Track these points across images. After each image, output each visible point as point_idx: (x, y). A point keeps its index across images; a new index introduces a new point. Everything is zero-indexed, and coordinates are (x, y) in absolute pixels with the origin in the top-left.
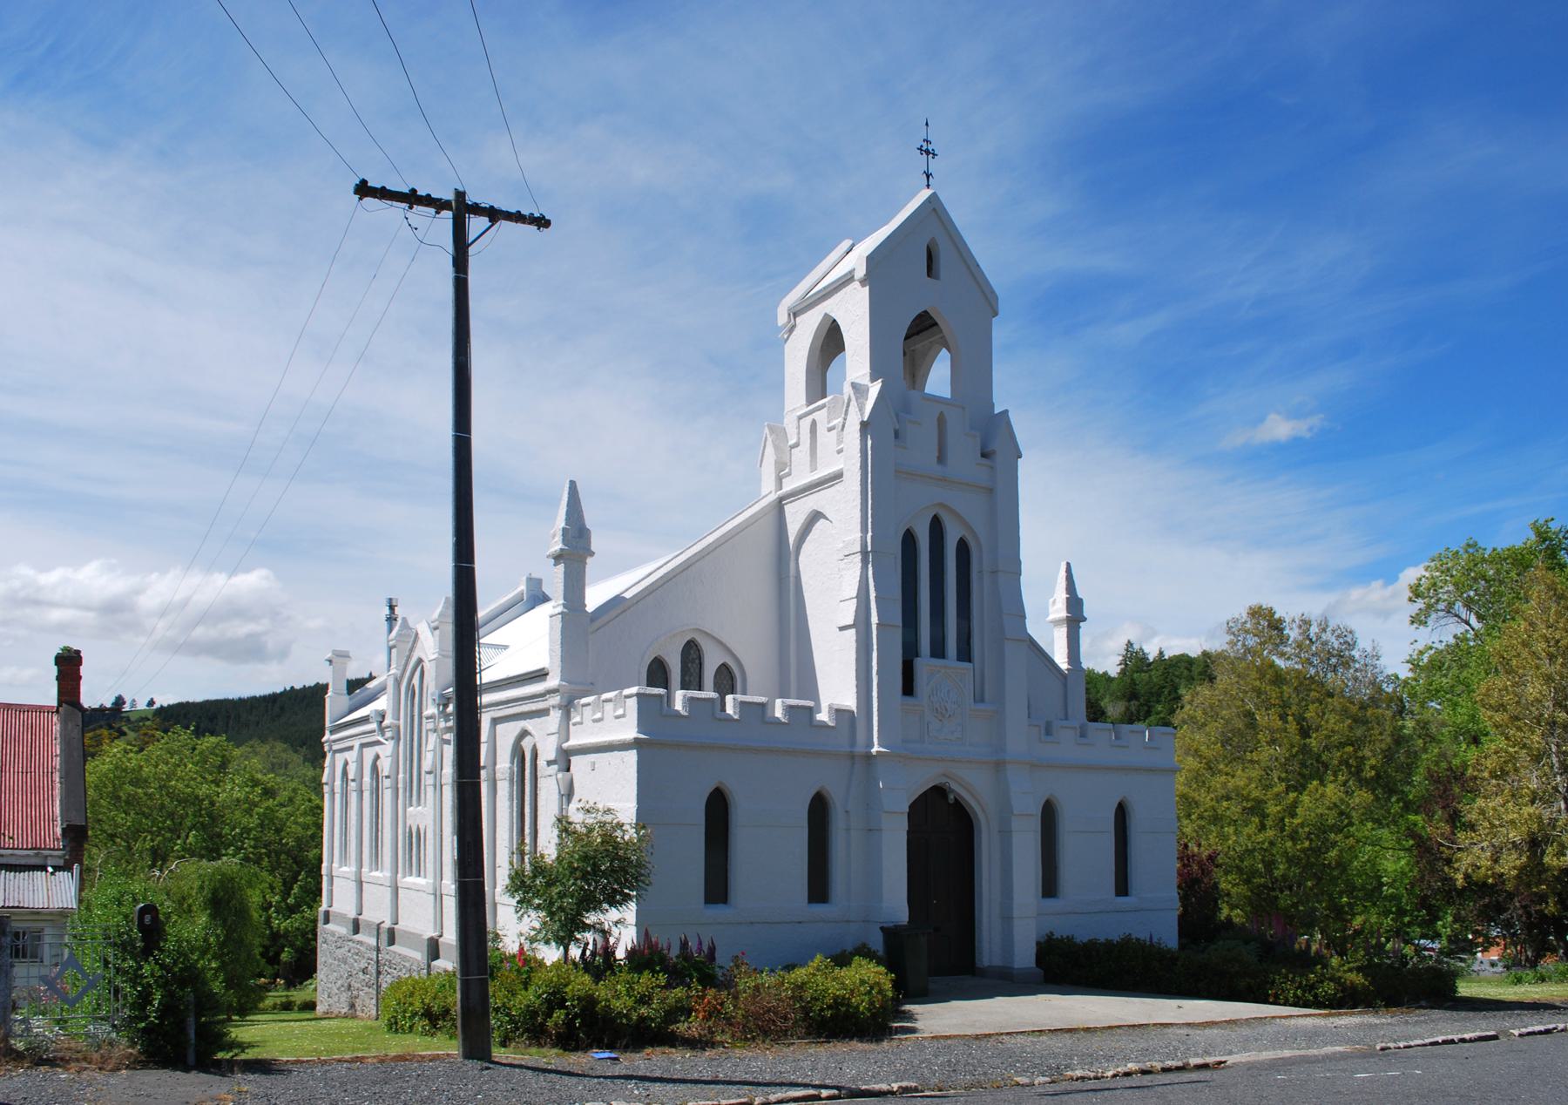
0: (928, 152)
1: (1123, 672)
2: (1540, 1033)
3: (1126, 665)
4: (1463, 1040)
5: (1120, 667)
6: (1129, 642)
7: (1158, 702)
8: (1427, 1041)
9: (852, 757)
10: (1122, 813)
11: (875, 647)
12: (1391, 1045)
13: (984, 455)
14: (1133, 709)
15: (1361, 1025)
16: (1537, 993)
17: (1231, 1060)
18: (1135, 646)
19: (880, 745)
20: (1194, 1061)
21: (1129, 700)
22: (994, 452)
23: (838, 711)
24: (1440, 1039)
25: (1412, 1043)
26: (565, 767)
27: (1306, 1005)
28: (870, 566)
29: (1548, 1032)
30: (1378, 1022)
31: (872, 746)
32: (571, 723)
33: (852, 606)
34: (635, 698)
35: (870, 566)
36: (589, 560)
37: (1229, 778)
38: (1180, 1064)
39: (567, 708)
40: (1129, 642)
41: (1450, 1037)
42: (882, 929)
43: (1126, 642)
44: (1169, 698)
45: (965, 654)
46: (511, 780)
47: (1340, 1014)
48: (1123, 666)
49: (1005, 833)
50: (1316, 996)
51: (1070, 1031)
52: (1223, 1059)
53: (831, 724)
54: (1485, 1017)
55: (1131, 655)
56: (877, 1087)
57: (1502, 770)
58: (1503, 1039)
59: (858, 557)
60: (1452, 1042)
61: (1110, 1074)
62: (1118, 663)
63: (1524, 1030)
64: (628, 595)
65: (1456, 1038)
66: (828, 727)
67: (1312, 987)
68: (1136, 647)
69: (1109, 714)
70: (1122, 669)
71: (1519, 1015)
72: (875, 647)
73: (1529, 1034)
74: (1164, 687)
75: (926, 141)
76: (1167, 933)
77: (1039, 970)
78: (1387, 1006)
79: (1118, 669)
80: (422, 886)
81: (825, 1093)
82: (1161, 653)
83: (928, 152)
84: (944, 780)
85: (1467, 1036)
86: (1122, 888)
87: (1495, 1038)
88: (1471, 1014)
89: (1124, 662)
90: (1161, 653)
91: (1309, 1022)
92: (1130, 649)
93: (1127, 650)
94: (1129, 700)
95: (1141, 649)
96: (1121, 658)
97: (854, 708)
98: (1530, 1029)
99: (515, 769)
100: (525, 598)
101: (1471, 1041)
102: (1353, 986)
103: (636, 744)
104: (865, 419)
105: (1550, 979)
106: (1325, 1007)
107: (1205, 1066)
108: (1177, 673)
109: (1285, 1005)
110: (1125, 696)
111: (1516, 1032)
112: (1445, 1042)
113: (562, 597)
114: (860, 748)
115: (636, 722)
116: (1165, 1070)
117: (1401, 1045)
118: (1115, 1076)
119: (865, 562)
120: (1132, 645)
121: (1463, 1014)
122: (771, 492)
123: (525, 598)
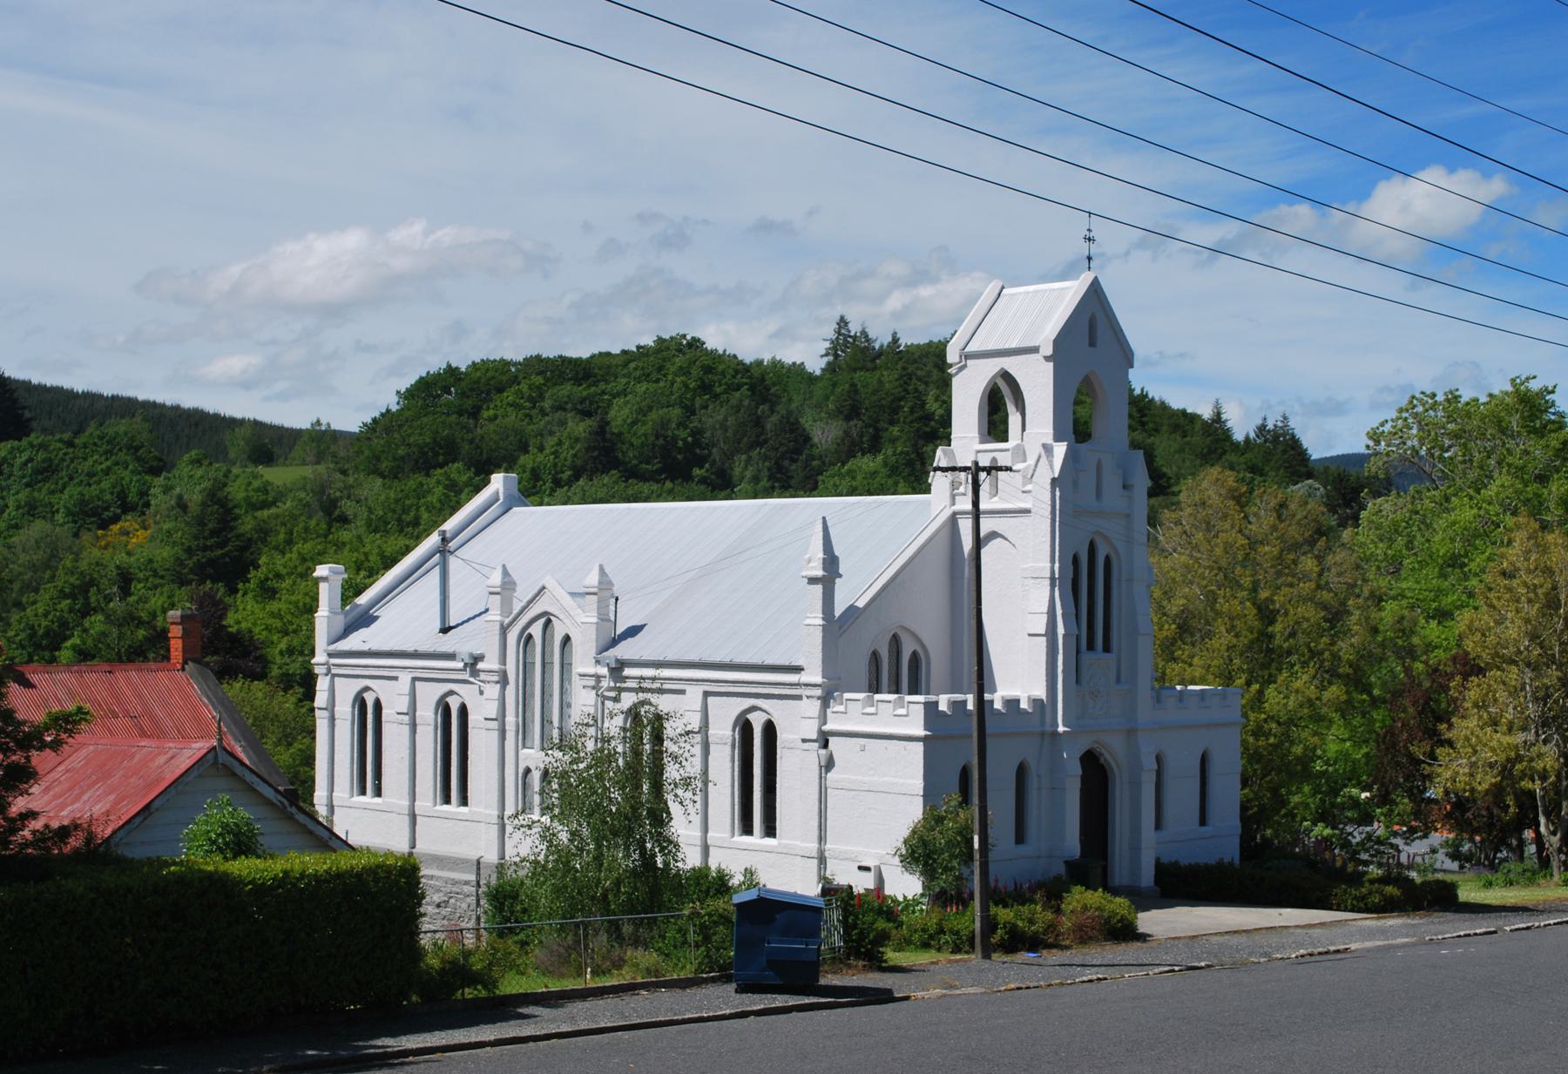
0: (1089, 239)
1: (831, 369)
2: (1523, 929)
3: (836, 356)
4: (1476, 934)
5: (826, 359)
6: (842, 318)
7: (892, 423)
8: (1455, 935)
9: (1043, 734)
10: (1204, 760)
11: (1061, 651)
12: (1434, 937)
13: (1125, 487)
14: (854, 433)
15: (1406, 925)
16: (1511, 898)
17: (1353, 946)
18: (851, 326)
19: (1064, 725)
20: (1332, 948)
21: (848, 418)
22: (1132, 486)
23: (1034, 700)
24: (1462, 933)
25: (1446, 936)
26: (823, 743)
27: (1359, 911)
28: (1057, 589)
29: (1528, 928)
30: (1413, 922)
31: (1058, 726)
32: (829, 711)
33: (1044, 619)
34: (922, 706)
35: (1057, 589)
36: (838, 581)
37: (1186, 666)
38: (1325, 950)
39: (826, 700)
40: (842, 318)
41: (1467, 932)
42: (1066, 862)
43: (838, 319)
44: (911, 418)
45: (1107, 648)
46: (733, 746)
47: (1385, 918)
48: (831, 358)
49: (1135, 785)
50: (1366, 904)
51: (1235, 932)
52: (1347, 946)
53: (1030, 711)
54: (1483, 919)
55: (845, 340)
56: (1196, 964)
57: (1483, 701)
58: (1500, 933)
59: (1047, 582)
60: (1469, 935)
61: (1294, 956)
62: (824, 352)
63: (1513, 927)
64: (861, 604)
65: (1472, 932)
66: (1028, 713)
67: (1363, 898)
68: (854, 328)
69: (816, 440)
70: (829, 363)
71: (1505, 916)
72: (1061, 651)
73: (1517, 930)
74: (900, 399)
75: (1089, 230)
76: (1230, 850)
77: (1158, 889)
78: (1413, 911)
79: (823, 363)
80: (776, 847)
81: (1176, 968)
82: (895, 340)
83: (1089, 239)
84: (1095, 746)
85: (1478, 931)
86: (1203, 822)
87: (1495, 932)
88: (1473, 916)
89: (835, 349)
90: (895, 340)
91: (1368, 923)
92: (843, 331)
93: (839, 333)
94: (848, 418)
95: (864, 333)
96: (827, 345)
97: (1044, 697)
98: (1517, 927)
99: (737, 736)
100: (501, 497)
101: (1481, 934)
102: (1392, 897)
103: (924, 739)
104: (1056, 476)
105: (1518, 883)
106: (1371, 912)
107: (1338, 951)
108: (919, 373)
109: (1344, 911)
110: (841, 412)
111: (1508, 929)
112: (1465, 935)
113: (821, 611)
114: (1048, 728)
115: (922, 723)
116: (1320, 953)
117: (1440, 937)
118: (1297, 957)
119: (1052, 586)
120: (846, 324)
121: (1467, 915)
122: (945, 507)
123: (501, 497)
